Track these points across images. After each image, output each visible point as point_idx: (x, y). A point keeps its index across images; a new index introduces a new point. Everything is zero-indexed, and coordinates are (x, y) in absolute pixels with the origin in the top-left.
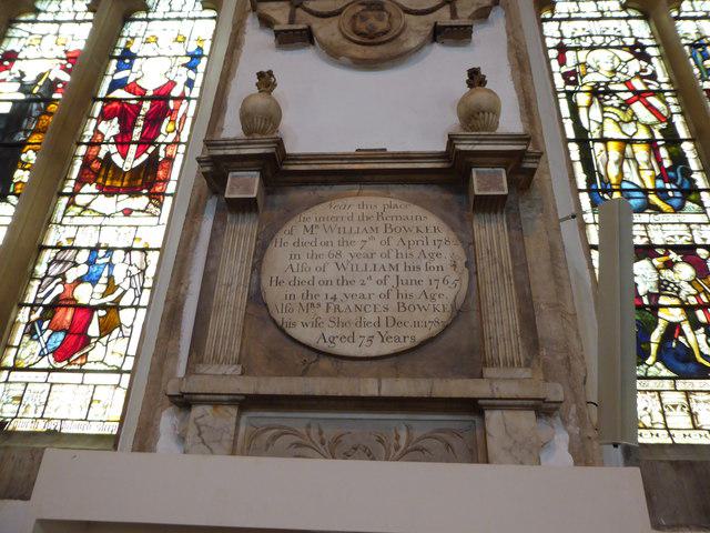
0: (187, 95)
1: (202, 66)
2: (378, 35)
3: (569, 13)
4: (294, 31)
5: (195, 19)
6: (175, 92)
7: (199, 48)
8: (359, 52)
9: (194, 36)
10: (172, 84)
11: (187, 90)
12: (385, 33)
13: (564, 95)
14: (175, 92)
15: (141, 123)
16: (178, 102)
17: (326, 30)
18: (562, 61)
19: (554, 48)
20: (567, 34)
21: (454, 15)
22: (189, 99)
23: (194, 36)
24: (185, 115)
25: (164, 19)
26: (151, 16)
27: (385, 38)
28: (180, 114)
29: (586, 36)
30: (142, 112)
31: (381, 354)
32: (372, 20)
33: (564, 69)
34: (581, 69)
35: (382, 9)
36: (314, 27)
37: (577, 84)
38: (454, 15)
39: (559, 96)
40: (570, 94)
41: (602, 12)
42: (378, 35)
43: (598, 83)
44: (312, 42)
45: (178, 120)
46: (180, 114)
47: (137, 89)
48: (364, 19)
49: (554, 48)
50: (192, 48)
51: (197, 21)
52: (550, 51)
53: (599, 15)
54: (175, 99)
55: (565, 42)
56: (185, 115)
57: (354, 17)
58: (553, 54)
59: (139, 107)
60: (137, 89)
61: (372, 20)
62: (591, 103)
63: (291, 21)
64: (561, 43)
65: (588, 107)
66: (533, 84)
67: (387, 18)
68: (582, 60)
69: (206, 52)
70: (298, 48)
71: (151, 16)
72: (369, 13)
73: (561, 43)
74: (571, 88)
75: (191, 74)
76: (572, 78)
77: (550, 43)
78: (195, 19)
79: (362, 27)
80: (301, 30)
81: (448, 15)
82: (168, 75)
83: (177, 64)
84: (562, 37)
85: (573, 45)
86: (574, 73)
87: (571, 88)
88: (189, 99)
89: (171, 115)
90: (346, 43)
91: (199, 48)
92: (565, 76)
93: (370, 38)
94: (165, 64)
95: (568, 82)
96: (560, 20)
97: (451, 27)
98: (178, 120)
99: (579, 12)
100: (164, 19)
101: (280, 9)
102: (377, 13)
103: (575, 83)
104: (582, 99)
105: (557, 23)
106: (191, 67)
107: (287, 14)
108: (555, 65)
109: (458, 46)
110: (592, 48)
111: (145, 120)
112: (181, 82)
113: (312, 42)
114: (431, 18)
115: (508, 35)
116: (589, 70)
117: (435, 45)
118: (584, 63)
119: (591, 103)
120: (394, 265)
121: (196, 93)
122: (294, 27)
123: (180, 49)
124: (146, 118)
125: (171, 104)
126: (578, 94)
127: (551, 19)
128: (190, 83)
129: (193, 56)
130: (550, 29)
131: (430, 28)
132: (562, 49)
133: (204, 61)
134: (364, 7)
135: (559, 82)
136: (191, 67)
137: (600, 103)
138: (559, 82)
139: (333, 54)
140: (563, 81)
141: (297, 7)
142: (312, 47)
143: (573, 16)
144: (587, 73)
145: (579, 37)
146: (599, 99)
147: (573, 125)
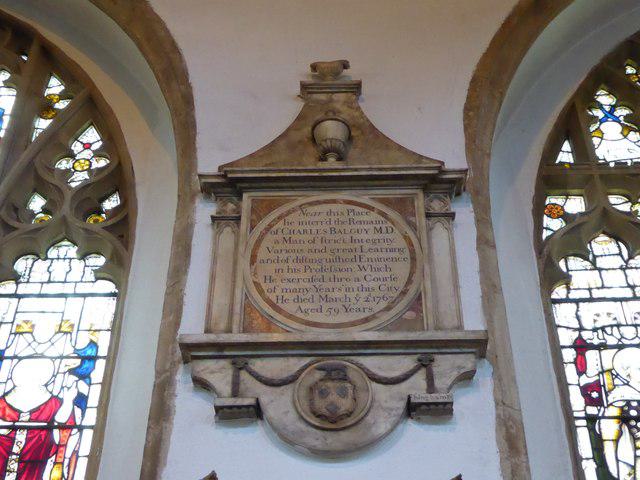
0: (78, 422)
1: (98, 372)
2: (341, 418)
3: (590, 289)
4: (239, 407)
5: (84, 296)
6: (62, 416)
7: (93, 344)
8: (315, 439)
9: (85, 325)
10: (56, 402)
11: (78, 412)
12: (349, 414)
13: (584, 422)
14: (62, 416)
15: (14, 466)
16: (66, 433)
17: (279, 405)
18: (581, 370)
19: (570, 347)
20: (588, 324)
21: (431, 388)
22: (81, 428)
23: (85, 325)
24: (76, 453)
25: (41, 296)
26: (22, 289)
27: (350, 421)
28: (69, 453)
29: (612, 326)
30: (16, 449)
31: (215, 360)
32: (333, 397)
33: (584, 380)
34: (607, 379)
35: (345, 379)
36: (264, 400)
37: (602, 405)
38: (431, 388)
39: (578, 423)
40: (592, 420)
41: (633, 287)
42: (341, 418)
43: (628, 403)
44: (262, 419)
45: (66, 462)
46: (69, 453)
47: (8, 411)
48: (324, 394)
49: (570, 347)
50: (83, 341)
51: (88, 299)
52: (564, 351)
53: (628, 293)
54: (62, 427)
55: (586, 335)
56: (76, 453)
57: (311, 389)
58: (569, 355)
59: (11, 439)
60: (8, 411)
61: (333, 397)
62: (620, 433)
63: (235, 393)
64: (580, 338)
65: (617, 441)
66: (528, 469)
67: (350, 391)
68: (607, 366)
69: (103, 351)
70: (245, 425)
71: (22, 289)
72: (330, 384)
73: (580, 338)
74: (592, 410)
75: (83, 387)
76: (595, 395)
77: (566, 337)
78: (84, 296)
79: (321, 405)
80: (248, 407)
81: (424, 384)
82: (50, 388)
83: (63, 369)
84: (581, 329)
85: (596, 342)
86: (597, 386)
87: (592, 410)
88: (81, 428)
89: (56, 453)
90: (302, 426)
91: (93, 344)
92: (585, 390)
93: (331, 421)
94: (44, 369)
95: (590, 401)
96: (577, 301)
97: (428, 404)
98: (66, 462)
99: (603, 287)
100: (41, 296)
101: (221, 370)
102: (338, 384)
103: (598, 402)
104: (609, 429)
105: (574, 306)
106: (82, 375)
107: (229, 378)
108: (571, 372)
109: (436, 424)
110: (620, 347)
111: (20, 461)
112: (69, 397)
113: (262, 419)
114: (403, 387)
115: (497, 404)
116: (617, 381)
117: (410, 421)
118: (610, 371)
119: (620, 433)
120: (323, 296)
121: (91, 417)
122: (239, 402)
123: (64, 346)
124: (22, 458)
125: (56, 435)
126: (602, 421)
127: (567, 300)
128: (81, 401)
129: (85, 359)
130: (564, 314)
131: (402, 405)
132: (581, 346)
133: (101, 365)
134: (323, 373)
135: (577, 401)
136: (82, 375)
137: (632, 434)
138: (577, 401)
139: (288, 441)
140: (583, 400)
141: (240, 369)
142: (259, 422)
143: (596, 294)
144: (615, 386)
145: (603, 329)
146: (630, 428)
147: (597, 470)
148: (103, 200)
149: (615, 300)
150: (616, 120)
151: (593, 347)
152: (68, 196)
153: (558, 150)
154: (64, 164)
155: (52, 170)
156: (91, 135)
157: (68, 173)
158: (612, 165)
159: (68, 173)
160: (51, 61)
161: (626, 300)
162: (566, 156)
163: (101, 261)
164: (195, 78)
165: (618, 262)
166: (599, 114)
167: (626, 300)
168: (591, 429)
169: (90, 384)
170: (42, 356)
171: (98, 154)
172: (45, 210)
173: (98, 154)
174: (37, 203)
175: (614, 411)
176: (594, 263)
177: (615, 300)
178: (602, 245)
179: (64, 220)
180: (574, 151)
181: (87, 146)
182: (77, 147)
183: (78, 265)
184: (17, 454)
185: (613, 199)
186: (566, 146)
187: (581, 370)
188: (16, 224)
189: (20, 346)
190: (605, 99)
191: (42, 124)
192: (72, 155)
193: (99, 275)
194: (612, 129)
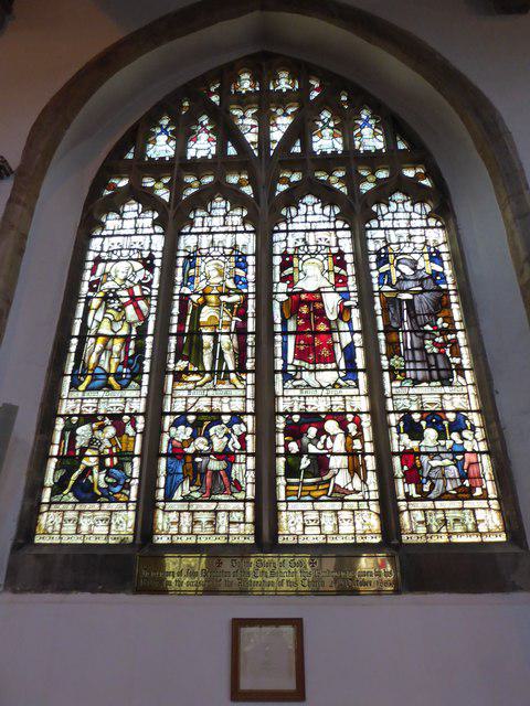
55: (102, 254)
62: (100, 306)
65: (96, 310)
74: (91, 294)
92: (91, 284)
110: (117, 261)
135: (85, 288)
149: (124, 235)
150: (329, 127)
151: (104, 261)
153: (226, 147)
158: (167, 159)
161: (131, 235)
162: (297, 149)
165: (222, 212)
166: (360, 123)
167: (131, 235)
168: (86, 303)
175: (101, 294)
176: (121, 216)
177: (124, 235)
178: (220, 205)
180: (301, 146)
184: (90, 336)
185: (318, 174)
186: (298, 143)
187: (93, 273)
190: (326, 115)
193: (337, 217)
194: (367, 132)
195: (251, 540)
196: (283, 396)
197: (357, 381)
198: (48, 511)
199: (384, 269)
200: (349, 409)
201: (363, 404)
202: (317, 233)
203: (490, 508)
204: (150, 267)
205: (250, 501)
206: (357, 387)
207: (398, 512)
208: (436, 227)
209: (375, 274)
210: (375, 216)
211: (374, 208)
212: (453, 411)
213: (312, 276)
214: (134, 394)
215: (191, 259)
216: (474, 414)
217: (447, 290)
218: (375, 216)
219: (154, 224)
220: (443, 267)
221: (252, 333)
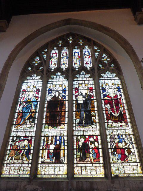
11: (121, 97)
14: (119, 97)
24: (123, 103)
112: (118, 95)
124: (115, 103)
148: (40, 67)
152: (34, 67)
154: (34, 62)
155: (32, 63)
156: (38, 58)
157: (35, 64)
159: (35, 64)
160: (95, 44)
163: (64, 76)
164: (131, 44)
169: (121, 93)
170: (111, 89)
171: (39, 61)
172: (113, 67)
173: (39, 61)
174: (30, 69)
178: (83, 73)
179: (34, 70)
181: (37, 59)
182: (36, 60)
183: (61, 76)
188: (26, 71)
189: (107, 87)
191: (97, 54)
192: (35, 61)
193: (64, 78)
195: (104, 176)
196: (76, 130)
197: (128, 125)
198: (77, 166)
199: (104, 93)
200: (94, 134)
201: (130, 132)
202: (115, 80)
203: (137, 166)
204: (119, 91)
205: (112, 163)
206: (34, 129)
207: (74, 168)
208: (91, 80)
209: (102, 95)
210: (102, 77)
211: (102, 75)
212: (87, 135)
213: (112, 93)
214: (33, 130)
215: (77, 89)
216: (132, 135)
217: (94, 100)
218: (102, 77)
219: (64, 78)
220: (22, 91)
221: (67, 111)
